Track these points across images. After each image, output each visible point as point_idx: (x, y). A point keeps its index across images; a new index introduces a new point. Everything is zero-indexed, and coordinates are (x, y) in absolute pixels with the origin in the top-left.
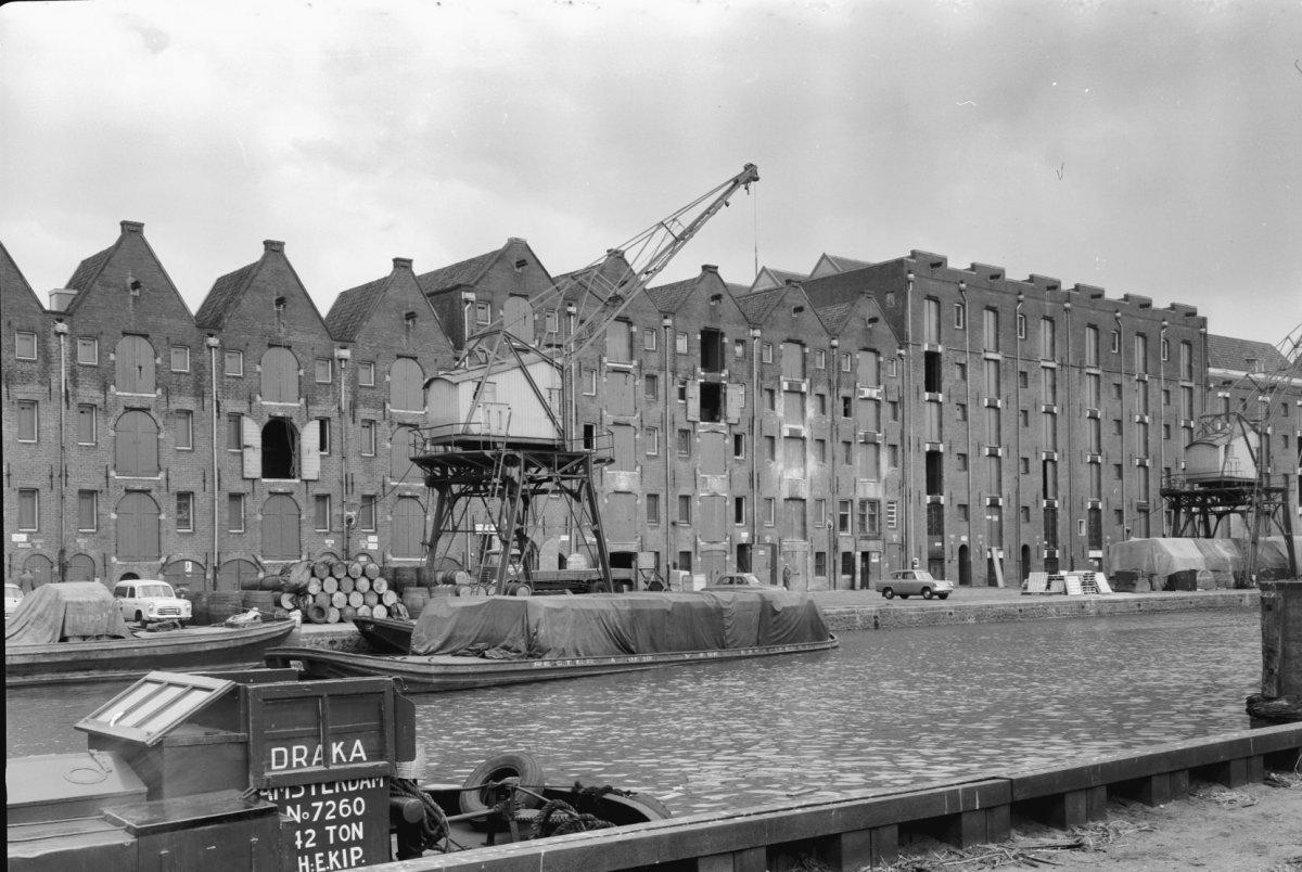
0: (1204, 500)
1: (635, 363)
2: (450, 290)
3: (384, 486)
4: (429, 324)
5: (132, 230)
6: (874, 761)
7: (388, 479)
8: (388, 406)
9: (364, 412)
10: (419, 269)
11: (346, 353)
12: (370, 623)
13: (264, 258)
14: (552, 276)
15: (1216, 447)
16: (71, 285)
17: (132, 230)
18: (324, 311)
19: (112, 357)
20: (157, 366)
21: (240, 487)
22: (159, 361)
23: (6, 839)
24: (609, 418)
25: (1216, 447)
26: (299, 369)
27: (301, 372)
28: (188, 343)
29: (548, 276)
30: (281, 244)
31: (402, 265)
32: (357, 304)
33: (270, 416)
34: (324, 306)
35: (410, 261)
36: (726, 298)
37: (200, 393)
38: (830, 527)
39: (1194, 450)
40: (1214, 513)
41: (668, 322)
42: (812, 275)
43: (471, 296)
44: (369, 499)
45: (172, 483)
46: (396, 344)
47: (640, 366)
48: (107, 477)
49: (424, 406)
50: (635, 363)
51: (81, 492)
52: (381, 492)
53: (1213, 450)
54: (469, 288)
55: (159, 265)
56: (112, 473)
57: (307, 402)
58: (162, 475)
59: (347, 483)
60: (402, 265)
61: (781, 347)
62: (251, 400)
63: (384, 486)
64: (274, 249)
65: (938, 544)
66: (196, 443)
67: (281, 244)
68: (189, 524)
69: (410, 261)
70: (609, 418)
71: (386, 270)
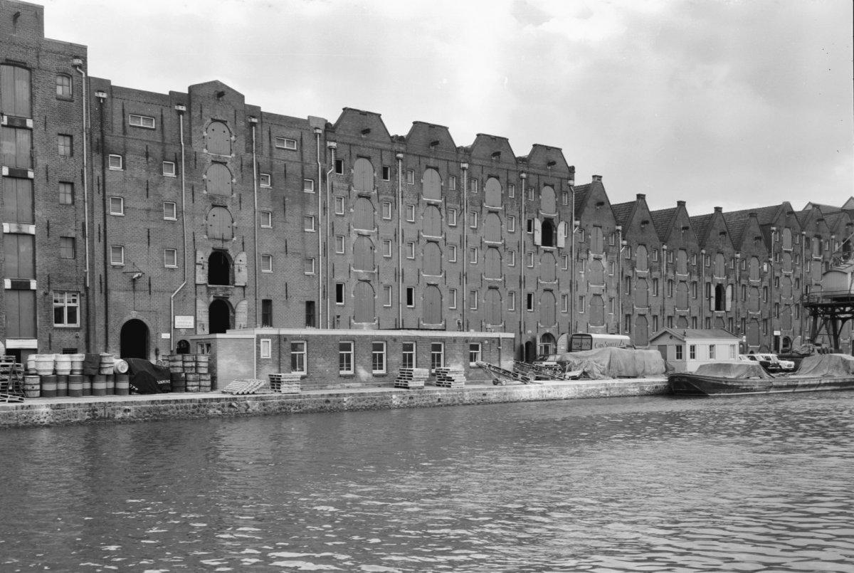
0: (833, 310)
1: (822, 256)
2: (766, 225)
6: (435, 515)
9: (743, 282)
11: (738, 255)
12: (676, 377)
15: (846, 274)
21: (709, 315)
24: (814, 282)
25: (846, 274)
31: (718, 209)
33: (213, 249)
37: (699, 275)
38: (459, 323)
39: (830, 275)
40: (841, 319)
41: (833, 237)
42: (844, 206)
43: (774, 228)
44: (743, 319)
46: (752, 251)
47: (823, 258)
50: (822, 256)
53: (844, 276)
54: (773, 225)
57: (650, 270)
58: (688, 310)
59: (737, 313)
60: (718, 209)
62: (712, 277)
69: (644, 195)
70: (814, 282)
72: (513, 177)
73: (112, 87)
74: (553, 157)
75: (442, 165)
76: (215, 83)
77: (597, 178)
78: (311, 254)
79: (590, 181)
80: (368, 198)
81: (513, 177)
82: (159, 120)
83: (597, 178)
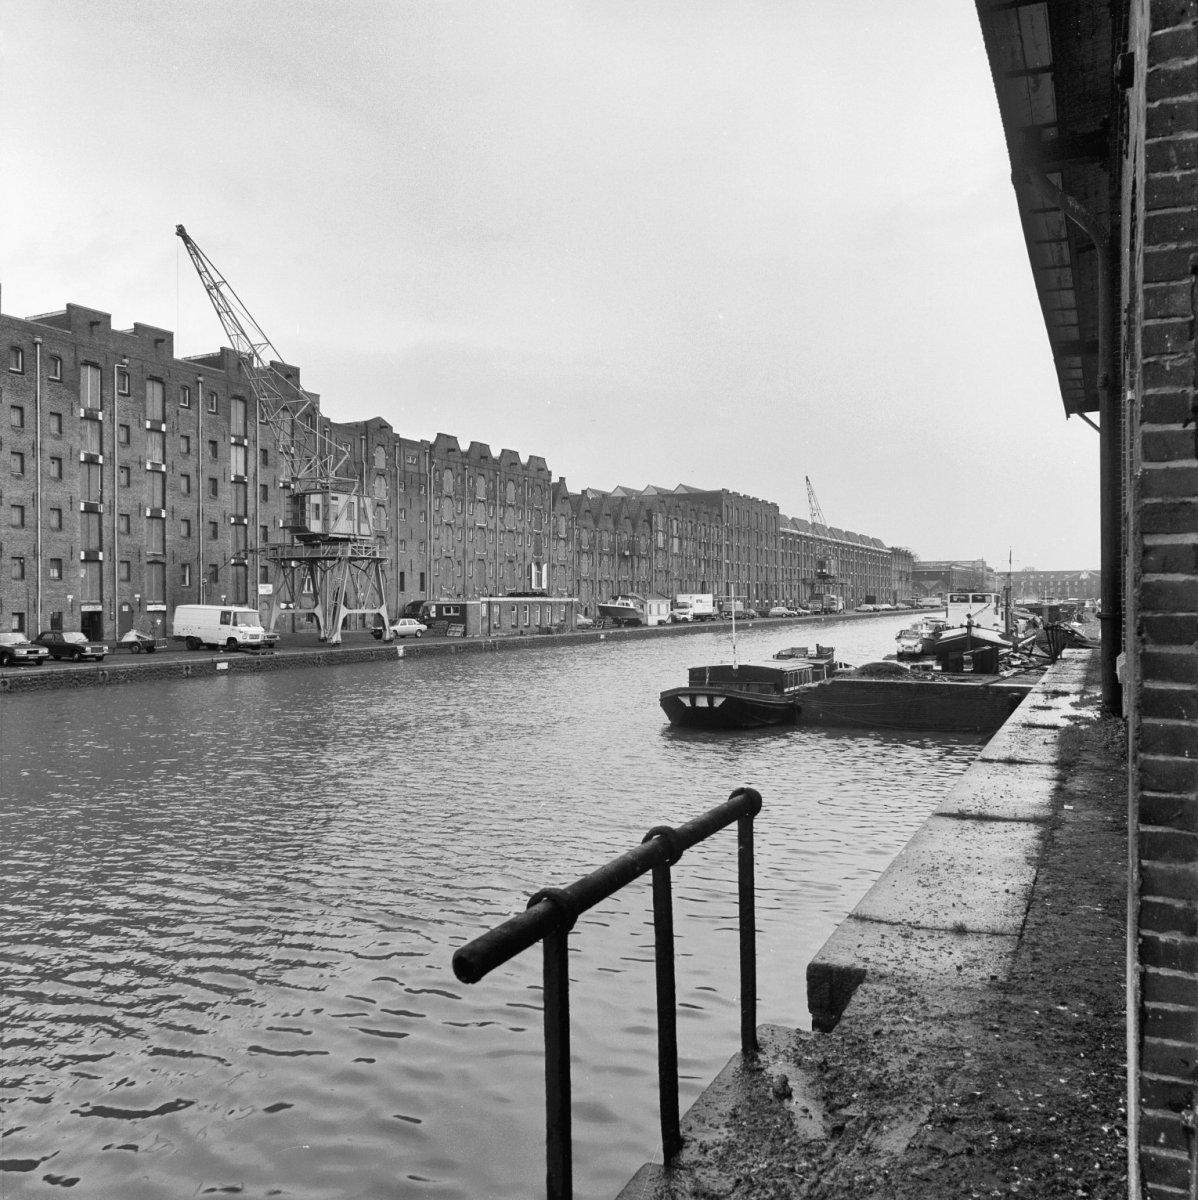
72: (521, 480)
73: (401, 439)
74: (541, 466)
75: (485, 472)
76: (378, 420)
77: (562, 479)
78: (423, 537)
79: (557, 480)
80: (450, 497)
83: (562, 479)
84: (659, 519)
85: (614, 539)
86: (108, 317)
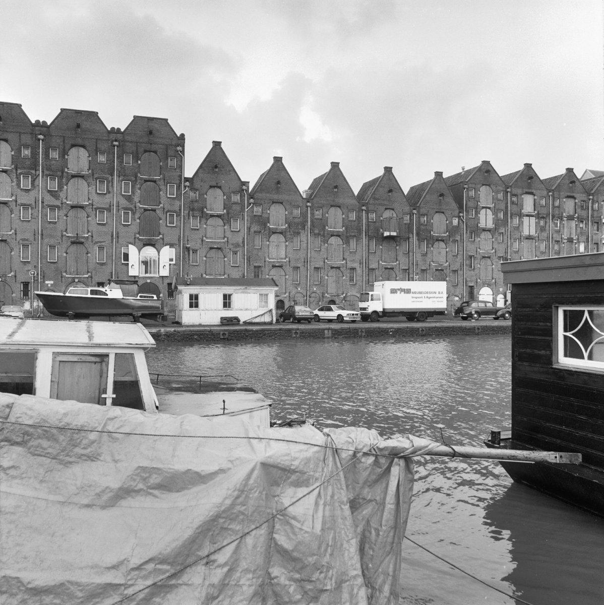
3: (430, 266)
4: (450, 200)
5: (388, 170)
7: (432, 263)
8: (432, 232)
10: (445, 176)
13: (384, 174)
14: (500, 175)
16: (309, 189)
17: (388, 170)
18: (406, 194)
19: (327, 215)
20: (343, 218)
22: (344, 216)
23: (516, 345)
26: (343, 215)
27: (448, 222)
28: (355, 209)
29: (498, 175)
30: (391, 168)
32: (418, 192)
34: (356, 190)
35: (281, 158)
36: (577, 183)
45: (348, 265)
48: (324, 262)
49: (11, 230)
51: (315, 268)
52: (428, 268)
55: (345, 179)
56: (326, 261)
60: (439, 174)
61: (564, 200)
63: (430, 266)
64: (335, 166)
65: (507, 315)
66: (357, 249)
67: (391, 168)
68: (354, 281)
71: (432, 177)
81: (104, 146)
82: (505, 211)
84: (485, 195)
85: (359, 218)
86: (97, 113)
